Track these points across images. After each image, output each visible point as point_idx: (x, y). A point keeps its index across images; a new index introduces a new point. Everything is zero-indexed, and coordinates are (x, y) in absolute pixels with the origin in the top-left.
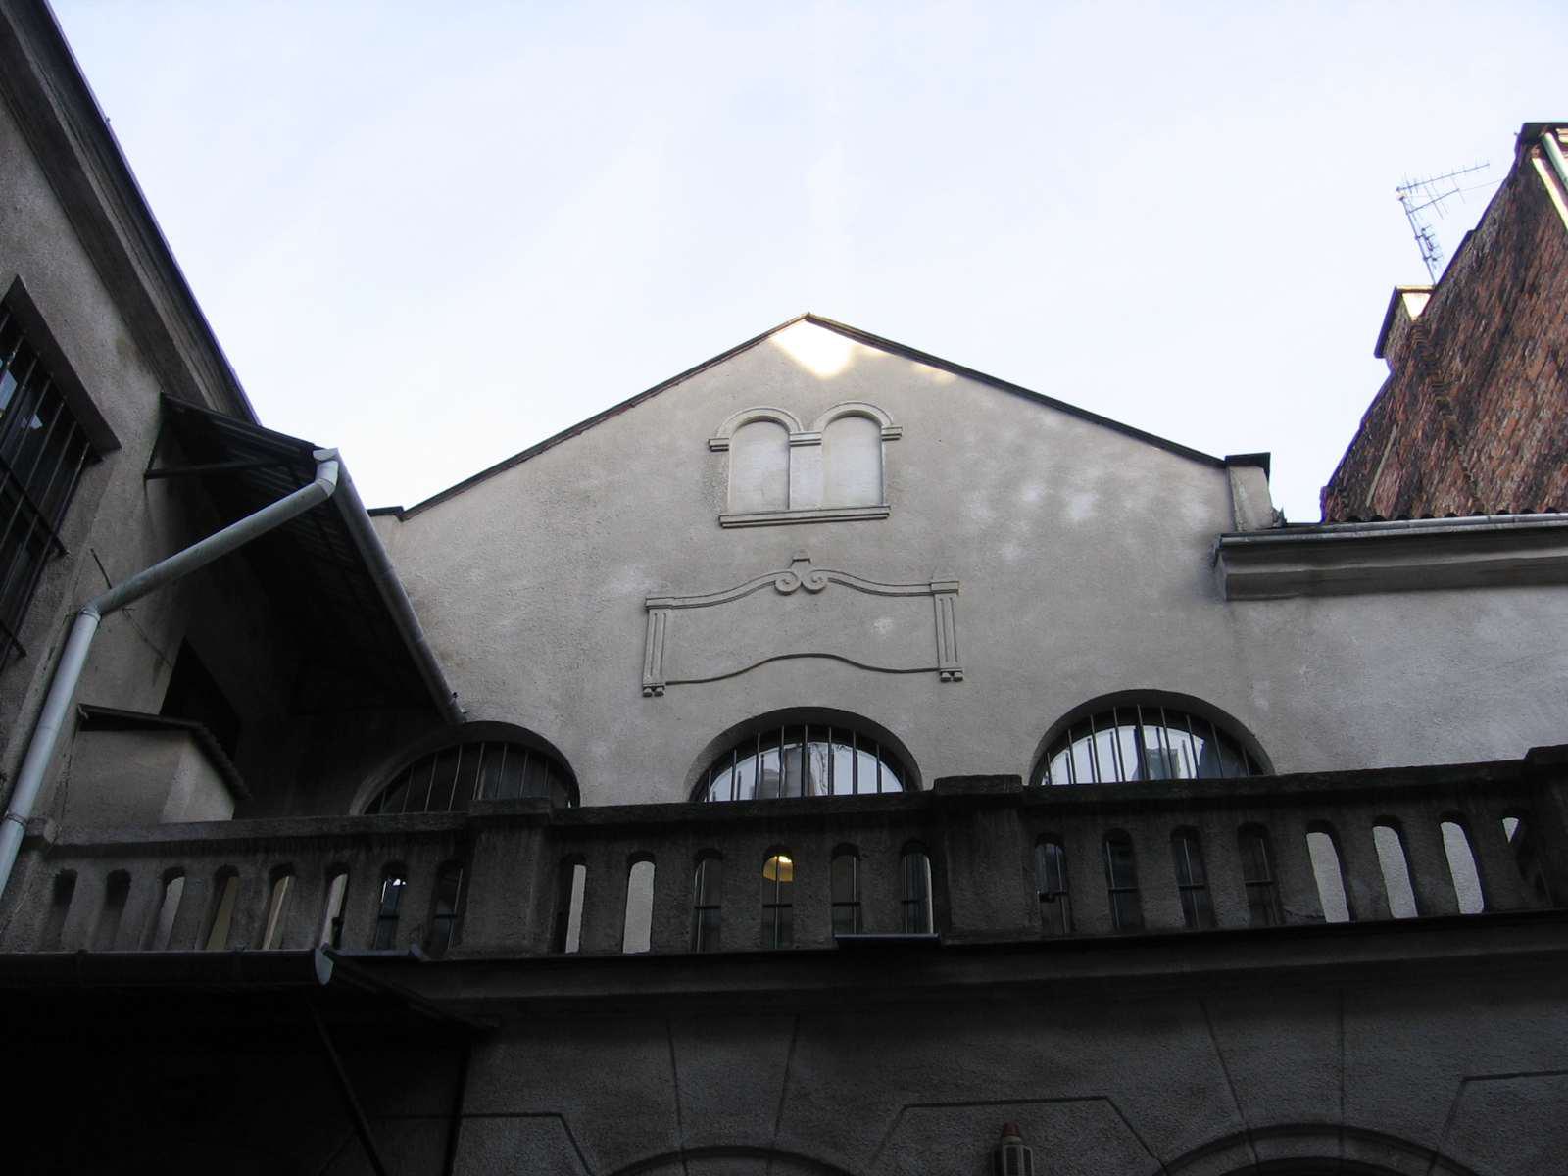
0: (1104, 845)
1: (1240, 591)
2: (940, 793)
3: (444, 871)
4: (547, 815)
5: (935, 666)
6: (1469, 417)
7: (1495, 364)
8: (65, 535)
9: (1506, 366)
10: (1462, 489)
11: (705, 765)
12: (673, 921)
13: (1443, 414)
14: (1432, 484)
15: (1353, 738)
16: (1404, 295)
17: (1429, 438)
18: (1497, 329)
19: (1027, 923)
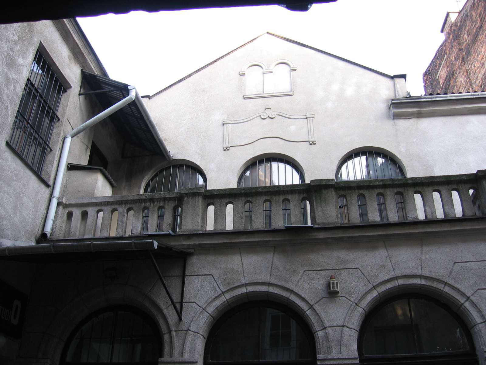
0: (358, 198)
1: (397, 116)
2: (312, 184)
3: (175, 210)
4: (203, 192)
5: (308, 140)
6: (468, 53)
7: (477, 37)
8: (59, 114)
9: (480, 38)
10: (466, 76)
11: (242, 170)
12: (239, 221)
13: (461, 52)
14: (456, 74)
15: (429, 160)
16: (450, 14)
17: (456, 59)
18: (478, 26)
19: (336, 220)
